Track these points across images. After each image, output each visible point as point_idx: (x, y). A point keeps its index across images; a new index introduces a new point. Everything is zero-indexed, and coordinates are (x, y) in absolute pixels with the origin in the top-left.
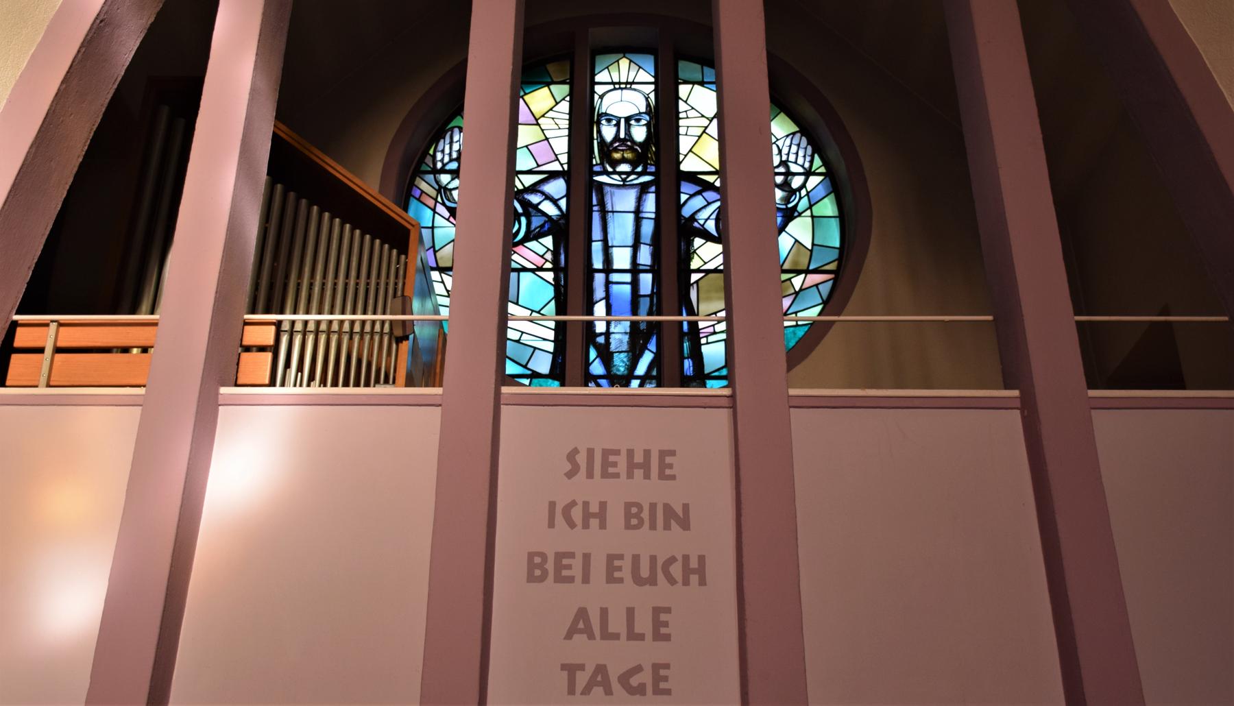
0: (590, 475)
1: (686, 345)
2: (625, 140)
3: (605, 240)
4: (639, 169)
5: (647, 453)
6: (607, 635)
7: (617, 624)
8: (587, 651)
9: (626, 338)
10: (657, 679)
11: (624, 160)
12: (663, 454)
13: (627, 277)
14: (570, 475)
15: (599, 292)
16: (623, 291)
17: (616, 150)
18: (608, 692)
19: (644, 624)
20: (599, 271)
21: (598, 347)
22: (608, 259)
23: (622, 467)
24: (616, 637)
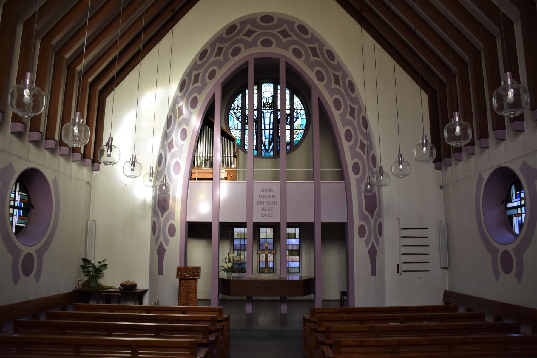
0: (264, 192)
1: (278, 144)
2: (268, 102)
3: (264, 123)
4: (270, 109)
5: (270, 189)
6: (266, 210)
7: (267, 209)
8: (264, 212)
9: (268, 143)
10: (271, 215)
11: (267, 107)
12: (272, 189)
13: (268, 131)
14: (262, 192)
15: (263, 134)
16: (267, 134)
17: (266, 105)
18: (266, 216)
19: (270, 209)
20: (263, 130)
21: (263, 144)
22: (265, 127)
23: (267, 191)
24: (267, 210)
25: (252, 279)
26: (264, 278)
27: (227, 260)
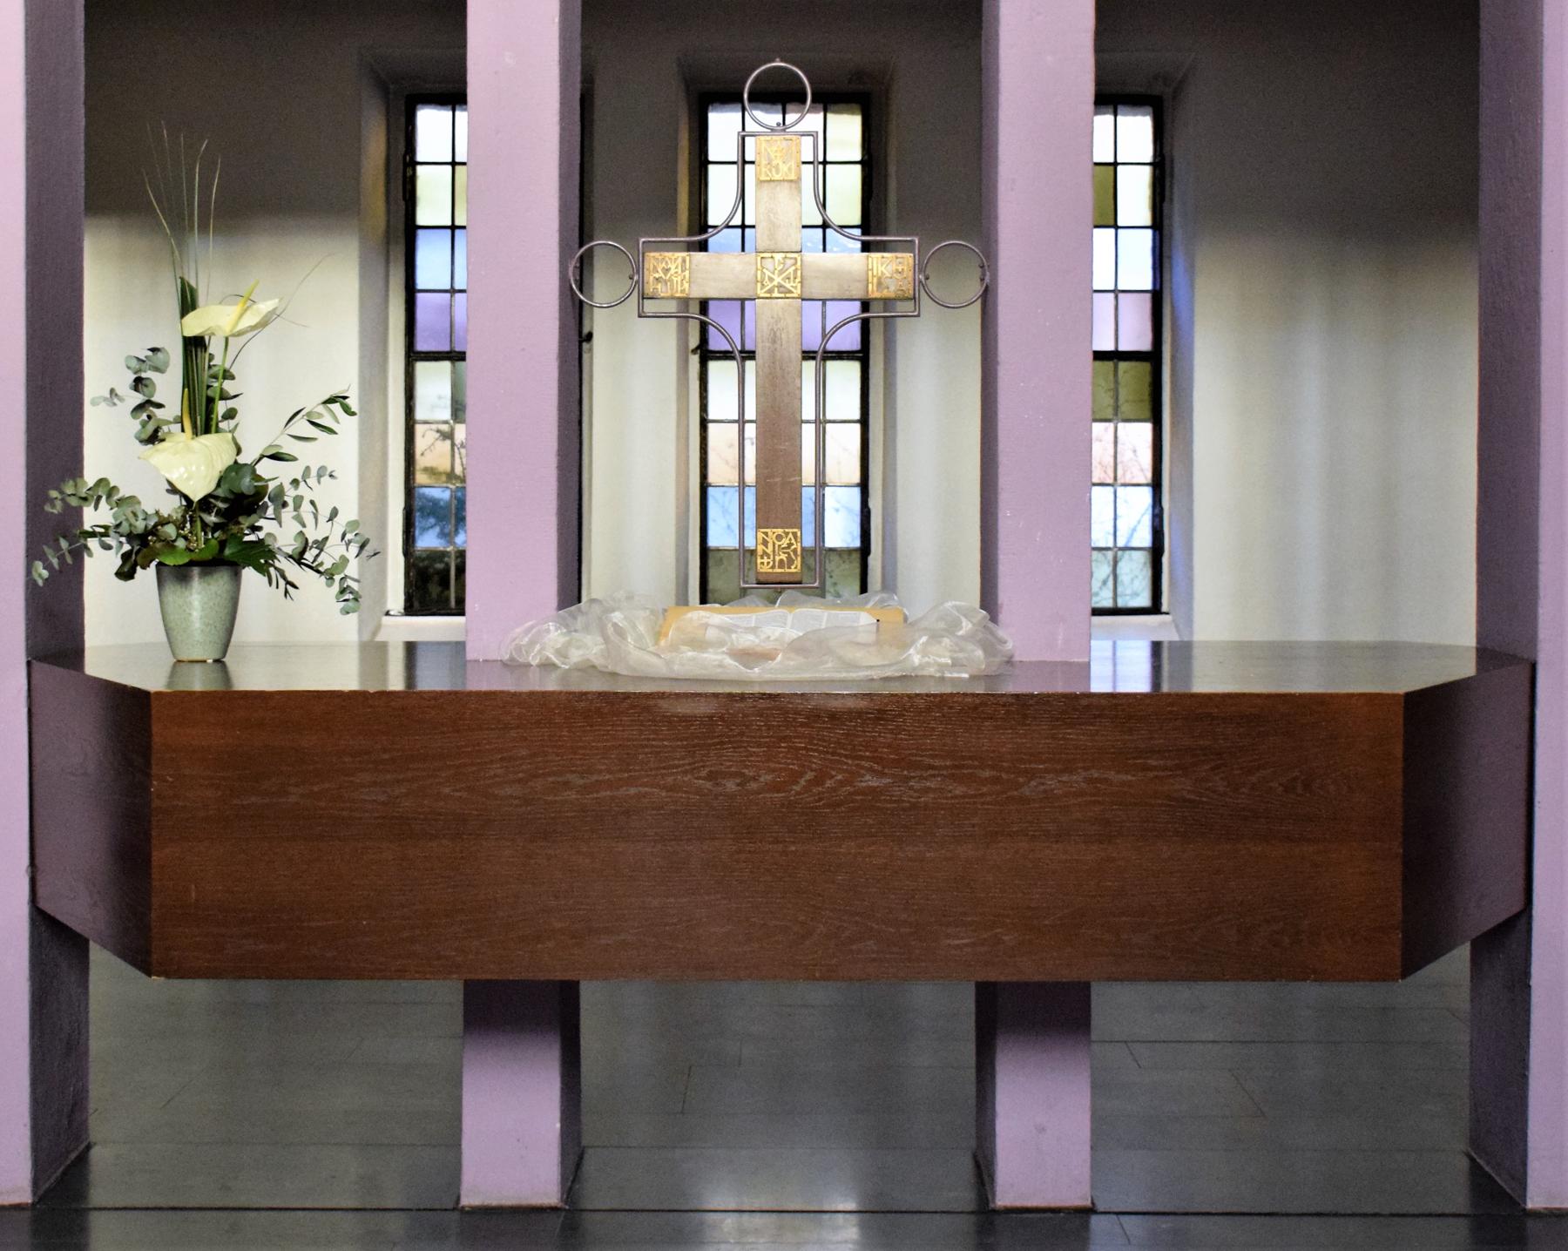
25: (551, 685)
26: (733, 668)
27: (169, 388)
